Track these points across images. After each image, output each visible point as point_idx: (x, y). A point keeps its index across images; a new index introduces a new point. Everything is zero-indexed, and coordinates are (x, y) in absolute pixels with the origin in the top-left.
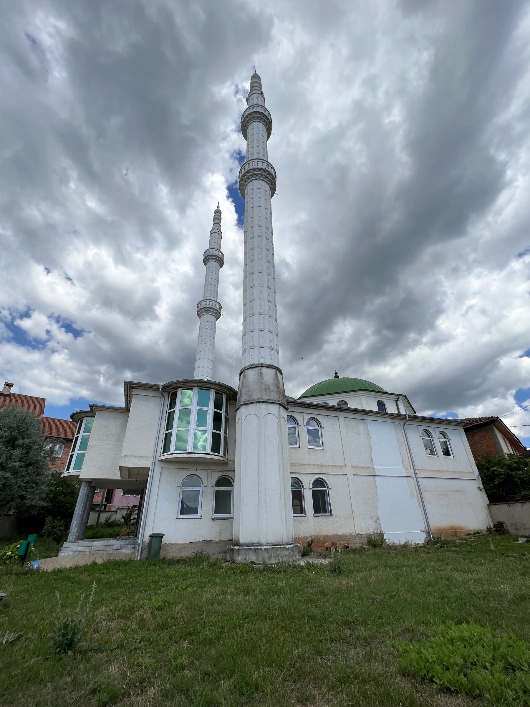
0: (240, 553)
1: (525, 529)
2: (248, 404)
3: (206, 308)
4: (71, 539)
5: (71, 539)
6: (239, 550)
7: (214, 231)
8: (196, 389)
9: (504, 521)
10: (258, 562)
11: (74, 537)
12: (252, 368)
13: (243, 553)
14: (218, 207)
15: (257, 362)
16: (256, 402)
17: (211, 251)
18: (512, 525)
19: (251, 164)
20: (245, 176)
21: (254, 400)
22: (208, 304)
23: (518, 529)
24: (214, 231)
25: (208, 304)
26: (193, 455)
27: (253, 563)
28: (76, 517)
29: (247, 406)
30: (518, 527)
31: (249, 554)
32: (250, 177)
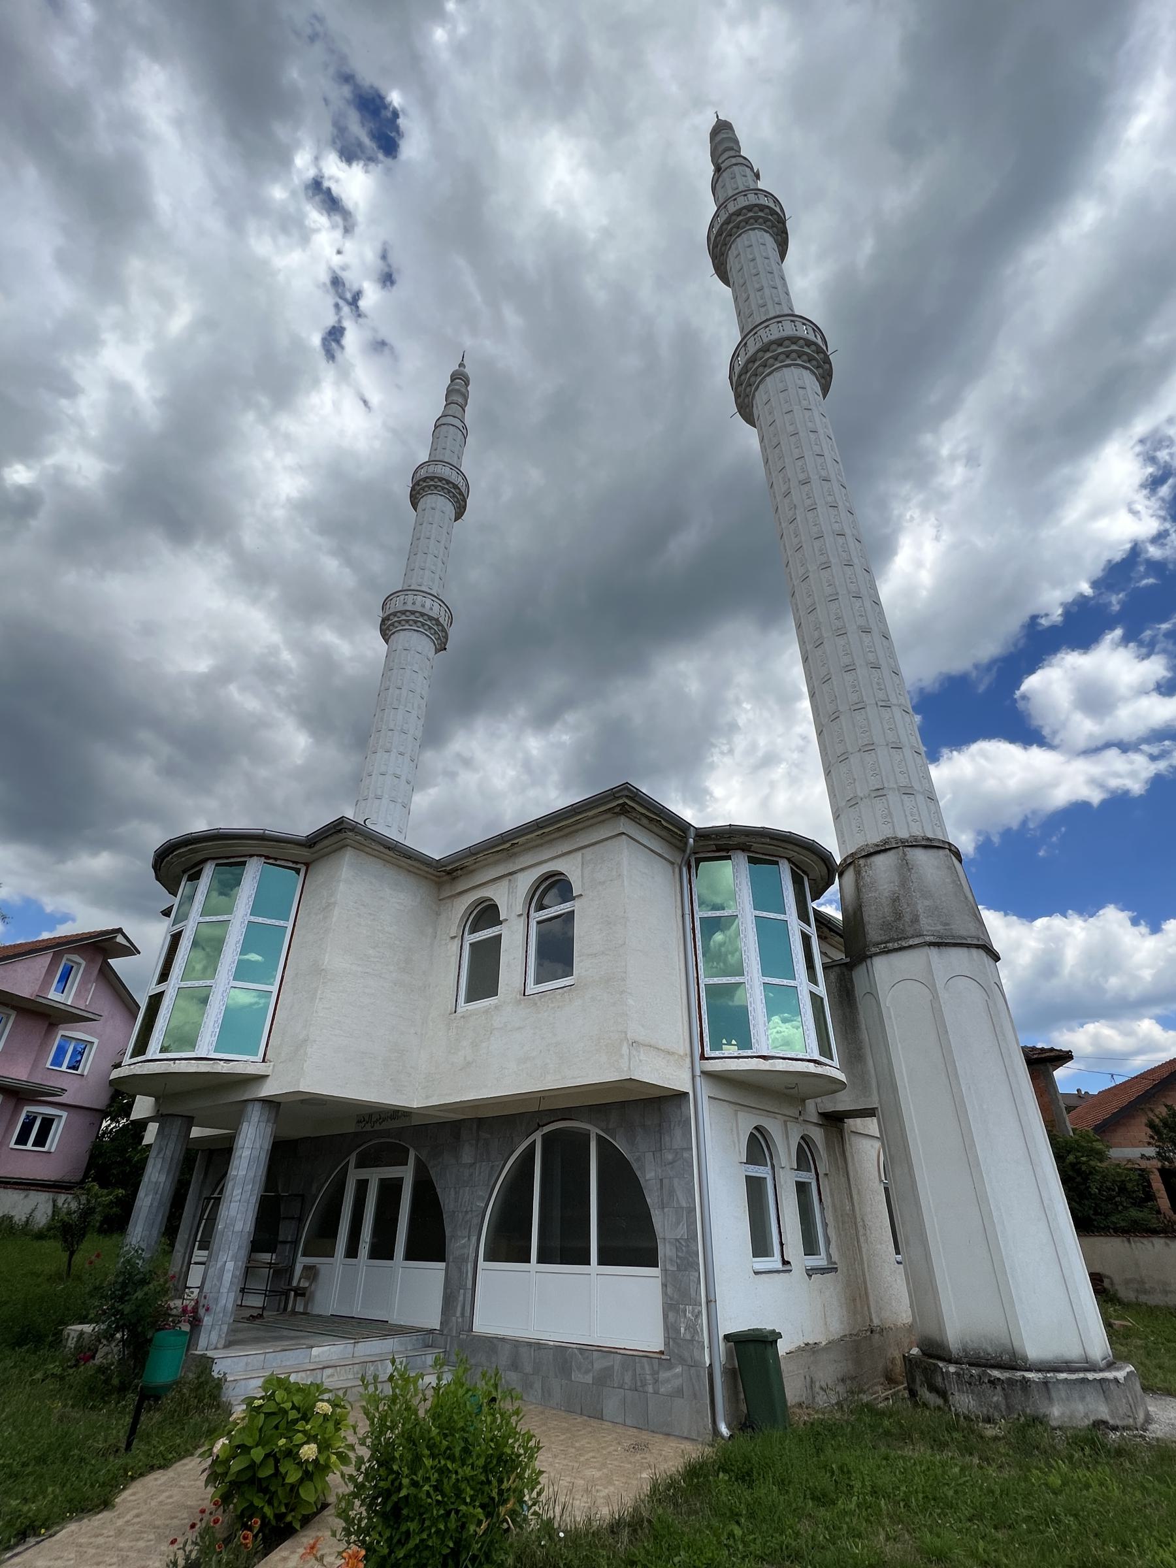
0: (1054, 1394)
1: (1166, 1292)
2: (947, 945)
3: (413, 613)
4: (214, 1336)
5: (214, 1336)
6: (1046, 1383)
7: (444, 420)
8: (741, 858)
9: (1107, 1273)
10: (1119, 1423)
11: (225, 1328)
12: (925, 847)
13: (1063, 1395)
14: (462, 365)
15: (903, 834)
16: (969, 946)
17: (431, 469)
18: (1127, 1282)
19: (774, 327)
20: (780, 345)
21: (953, 937)
22: (410, 602)
23: (1145, 1292)
24: (444, 420)
25: (410, 602)
26: (781, 1066)
27: (1099, 1424)
28: (234, 1247)
29: (943, 949)
30: (1147, 1286)
31: (1083, 1399)
32: (782, 357)
